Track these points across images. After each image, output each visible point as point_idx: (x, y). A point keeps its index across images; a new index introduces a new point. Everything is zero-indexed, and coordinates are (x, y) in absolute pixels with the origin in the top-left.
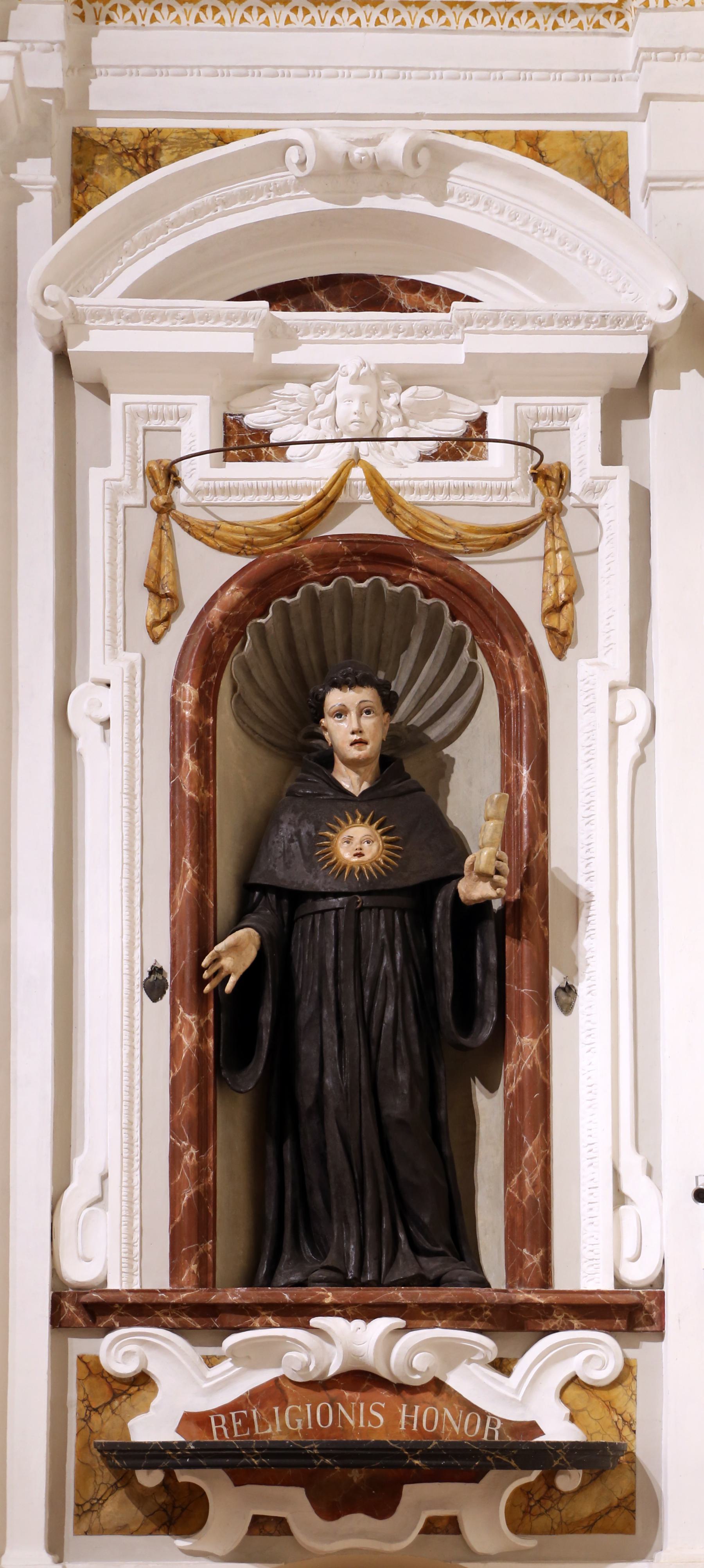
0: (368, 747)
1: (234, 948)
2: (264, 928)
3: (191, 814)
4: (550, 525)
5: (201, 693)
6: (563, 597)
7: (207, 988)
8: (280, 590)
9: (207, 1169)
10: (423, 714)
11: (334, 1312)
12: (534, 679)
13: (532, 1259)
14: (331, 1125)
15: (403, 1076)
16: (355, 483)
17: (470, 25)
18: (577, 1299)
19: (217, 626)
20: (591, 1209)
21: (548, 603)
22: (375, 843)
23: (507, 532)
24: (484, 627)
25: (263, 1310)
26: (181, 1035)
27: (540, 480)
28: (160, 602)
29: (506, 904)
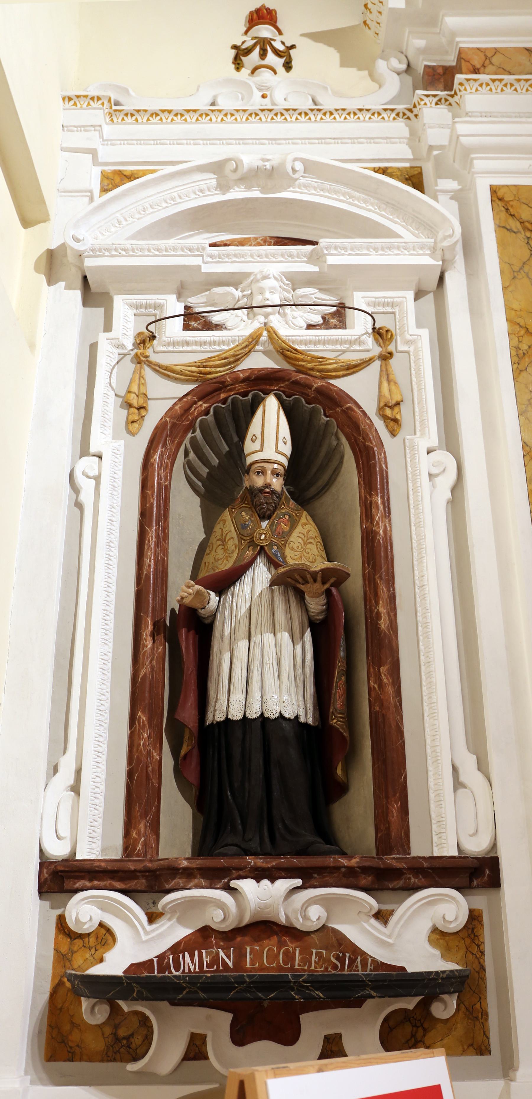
17: (150, 120)
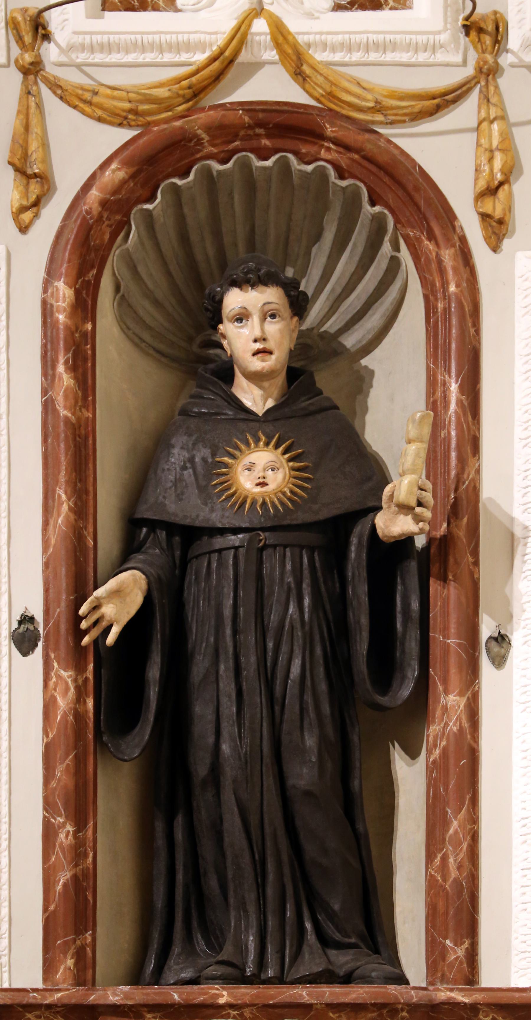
0: (273, 357)
1: (117, 593)
2: (152, 571)
3: (66, 436)
4: (484, 89)
5: (78, 293)
6: (499, 177)
7: (86, 640)
8: (170, 170)
9: (86, 850)
10: (337, 319)
11: (229, 1014)
12: (465, 276)
13: (455, 952)
14: (228, 796)
15: (310, 741)
16: (258, 38)
18: (505, 999)
19: (95, 212)
20: (524, 894)
21: (482, 184)
22: (281, 470)
23: (434, 98)
24: (408, 214)
25: (149, 1012)
26: (56, 694)
27: (473, 34)
28: (28, 183)
29: (430, 541)
